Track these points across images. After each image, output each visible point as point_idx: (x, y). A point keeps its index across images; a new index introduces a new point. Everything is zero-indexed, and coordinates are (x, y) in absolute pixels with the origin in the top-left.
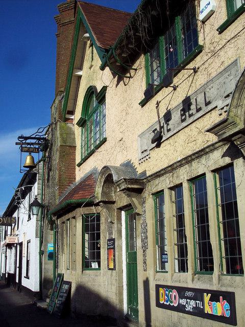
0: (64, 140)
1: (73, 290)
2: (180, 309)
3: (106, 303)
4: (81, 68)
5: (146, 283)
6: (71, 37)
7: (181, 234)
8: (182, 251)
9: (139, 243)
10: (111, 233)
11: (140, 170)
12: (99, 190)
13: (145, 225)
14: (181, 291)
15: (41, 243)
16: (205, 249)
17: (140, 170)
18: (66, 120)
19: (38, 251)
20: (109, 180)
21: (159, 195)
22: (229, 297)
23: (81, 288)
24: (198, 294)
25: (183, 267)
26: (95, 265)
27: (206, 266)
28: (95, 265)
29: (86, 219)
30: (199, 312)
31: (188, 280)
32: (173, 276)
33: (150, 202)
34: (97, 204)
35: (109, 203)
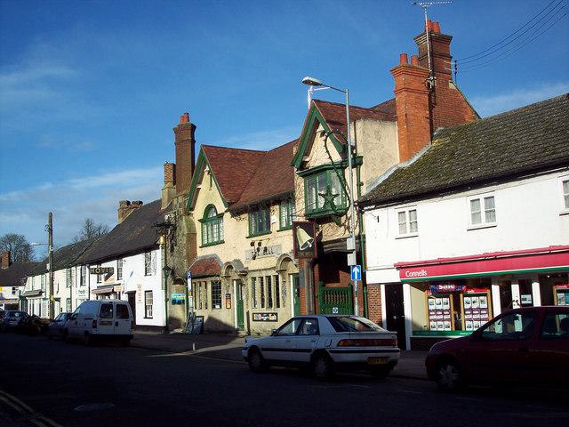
0: (189, 230)
1: (205, 320)
2: (262, 320)
3: (225, 325)
4: (200, 183)
5: (248, 313)
6: (321, 387)
7: (262, 295)
8: (263, 300)
9: (244, 297)
10: (228, 291)
11: (245, 266)
12: (223, 271)
13: (247, 292)
14: (262, 314)
15: (166, 293)
16: (270, 300)
17: (245, 266)
18: (189, 214)
19: (164, 298)
20: (230, 267)
21: (254, 279)
22: (276, 314)
23: (210, 319)
24: (268, 314)
25: (263, 307)
26: (218, 307)
27: (271, 305)
28: (218, 307)
29: (213, 283)
30: (268, 320)
31: (264, 310)
32: (259, 309)
33: (250, 281)
34: (39, 269)
35: (227, 277)
